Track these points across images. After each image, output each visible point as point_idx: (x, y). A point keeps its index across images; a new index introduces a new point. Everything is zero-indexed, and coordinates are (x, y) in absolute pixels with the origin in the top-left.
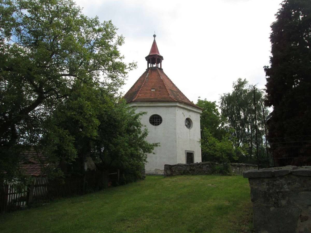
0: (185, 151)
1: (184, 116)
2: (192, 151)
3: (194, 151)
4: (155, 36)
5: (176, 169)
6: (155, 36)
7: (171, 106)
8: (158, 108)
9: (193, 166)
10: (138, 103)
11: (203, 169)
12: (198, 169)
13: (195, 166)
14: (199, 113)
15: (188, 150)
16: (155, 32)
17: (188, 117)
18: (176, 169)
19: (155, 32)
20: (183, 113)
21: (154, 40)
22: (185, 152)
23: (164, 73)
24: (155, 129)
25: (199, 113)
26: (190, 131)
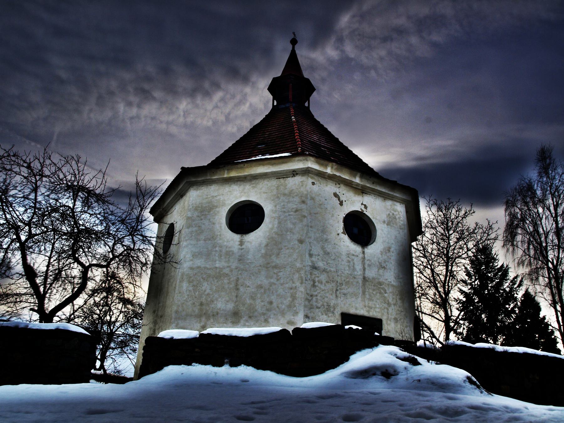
1: (341, 204)
17: (357, 207)
20: (336, 195)
26: (364, 253)
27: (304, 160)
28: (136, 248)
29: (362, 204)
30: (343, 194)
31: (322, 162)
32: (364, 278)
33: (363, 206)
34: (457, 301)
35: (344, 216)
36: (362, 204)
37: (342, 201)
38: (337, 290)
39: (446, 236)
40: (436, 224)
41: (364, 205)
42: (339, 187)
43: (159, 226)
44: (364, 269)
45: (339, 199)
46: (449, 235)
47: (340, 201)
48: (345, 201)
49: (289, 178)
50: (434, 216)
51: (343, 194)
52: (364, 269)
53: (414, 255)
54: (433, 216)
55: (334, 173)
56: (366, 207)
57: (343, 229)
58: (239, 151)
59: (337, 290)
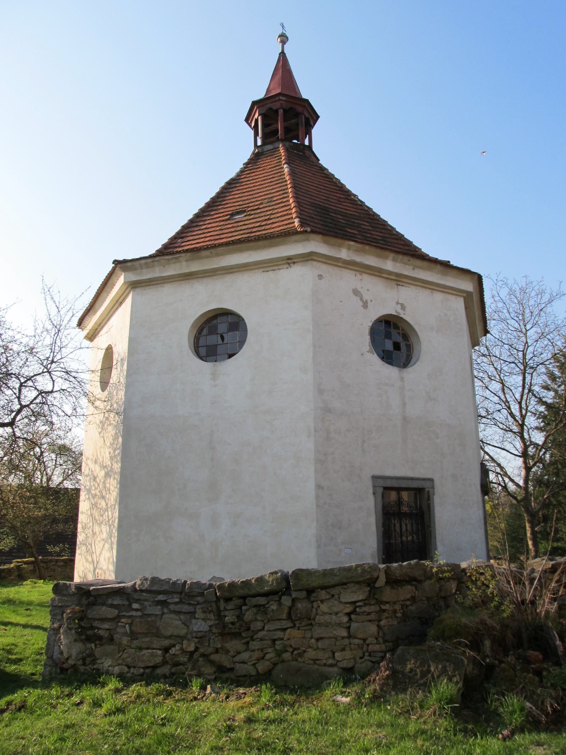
0: (375, 478)
1: (365, 305)
2: (418, 479)
3: (431, 480)
4: (284, 39)
5: (117, 618)
6: (284, 39)
7: (289, 258)
8: (229, 278)
9: (244, 598)
10: (141, 268)
11: (318, 632)
12: (277, 625)
13: (255, 601)
14: (457, 292)
15: (389, 472)
16: (283, 26)
17: (390, 309)
18: (117, 618)
19: (283, 26)
20: (356, 292)
21: (282, 54)
22: (374, 487)
23: (322, 169)
24: (214, 376)
25: (457, 292)
26: (402, 379)
27: (304, 240)
28: (56, 388)
29: (397, 303)
30: (368, 290)
31: (334, 240)
32: (405, 419)
33: (399, 306)
34: (535, 414)
35: (371, 324)
36: (397, 303)
37: (366, 301)
38: (364, 442)
39: (521, 331)
40: (507, 315)
41: (400, 304)
42: (361, 280)
43: (256, 158)
44: (404, 404)
45: (361, 299)
46: (527, 331)
47: (363, 302)
48: (371, 301)
49: (281, 270)
50: (504, 303)
51: (368, 290)
52: (404, 404)
53: (476, 384)
54: (502, 304)
55: (353, 258)
56: (403, 307)
57: (370, 346)
58: (225, 202)
59: (364, 442)
